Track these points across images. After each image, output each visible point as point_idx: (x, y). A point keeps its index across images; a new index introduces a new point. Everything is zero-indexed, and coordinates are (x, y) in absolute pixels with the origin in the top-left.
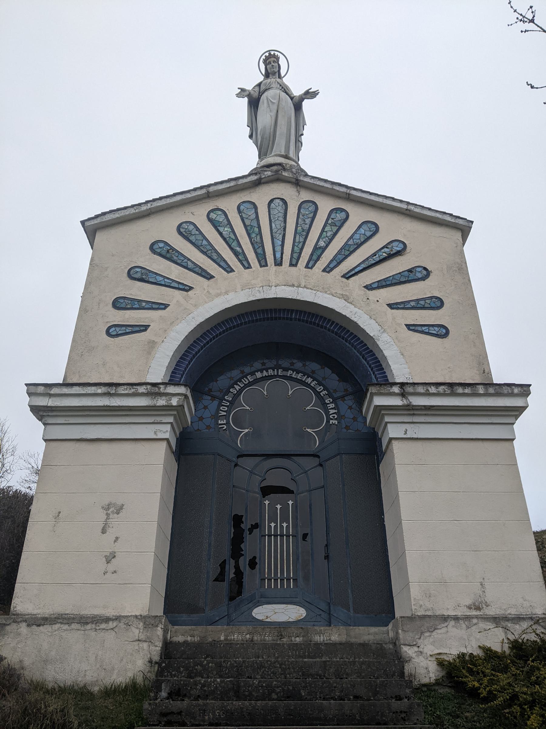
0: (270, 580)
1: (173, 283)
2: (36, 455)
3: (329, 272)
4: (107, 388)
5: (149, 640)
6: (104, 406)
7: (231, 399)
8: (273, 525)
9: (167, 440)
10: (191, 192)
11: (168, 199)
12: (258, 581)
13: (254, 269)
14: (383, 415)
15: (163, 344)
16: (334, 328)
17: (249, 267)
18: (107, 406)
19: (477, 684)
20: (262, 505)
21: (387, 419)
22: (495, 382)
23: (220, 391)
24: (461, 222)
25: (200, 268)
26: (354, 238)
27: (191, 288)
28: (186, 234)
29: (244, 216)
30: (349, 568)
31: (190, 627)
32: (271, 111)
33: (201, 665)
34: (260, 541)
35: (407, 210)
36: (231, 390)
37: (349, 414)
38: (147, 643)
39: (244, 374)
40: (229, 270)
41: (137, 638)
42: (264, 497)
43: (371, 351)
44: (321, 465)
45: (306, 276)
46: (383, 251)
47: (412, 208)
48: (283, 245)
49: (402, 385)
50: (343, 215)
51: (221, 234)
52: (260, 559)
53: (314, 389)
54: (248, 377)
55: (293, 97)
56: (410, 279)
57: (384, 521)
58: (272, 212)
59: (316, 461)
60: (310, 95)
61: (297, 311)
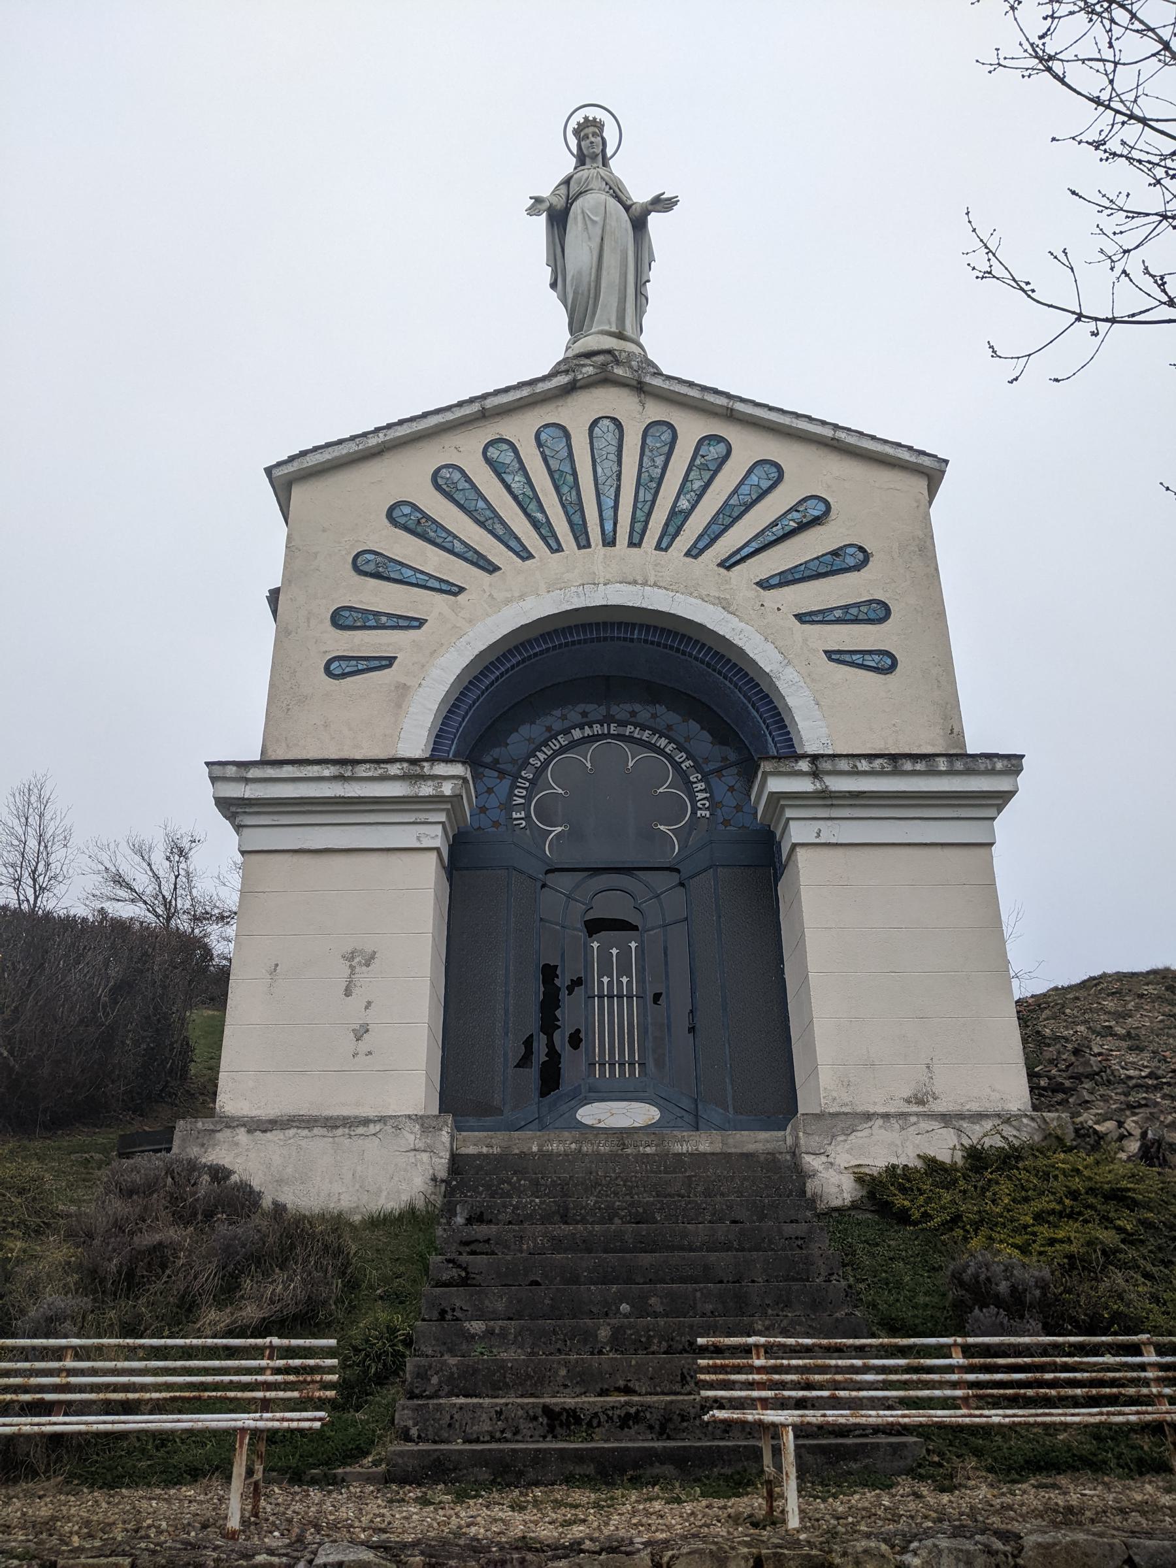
0: (602, 1065)
1: (431, 580)
2: (112, 846)
3: (696, 557)
4: (338, 767)
5: (429, 1149)
6: (335, 797)
7: (531, 776)
8: (605, 980)
9: (437, 849)
10: (454, 409)
11: (414, 424)
12: (584, 1067)
13: (567, 552)
14: (783, 807)
15: (421, 689)
16: (706, 655)
17: (559, 549)
18: (340, 797)
19: (906, 1203)
20: (588, 949)
21: (789, 813)
22: (969, 752)
23: (514, 761)
24: (926, 461)
25: (476, 552)
26: (739, 492)
27: (462, 590)
28: (447, 489)
29: (547, 452)
30: (727, 1045)
31: (485, 1134)
32: (590, 238)
33: (509, 1183)
34: (586, 1006)
35: (833, 439)
36: (531, 760)
37: (730, 800)
38: (427, 1154)
39: (553, 732)
40: (524, 555)
41: (412, 1146)
42: (590, 936)
43: (767, 696)
44: (682, 884)
45: (656, 565)
46: (790, 517)
47: (842, 435)
48: (616, 508)
49: (815, 758)
50: (721, 448)
51: (508, 488)
52: (586, 1034)
53: (670, 757)
54: (559, 738)
55: (631, 206)
56: (834, 568)
57: (783, 973)
58: (595, 444)
59: (674, 878)
60: (662, 204)
61: (641, 626)
